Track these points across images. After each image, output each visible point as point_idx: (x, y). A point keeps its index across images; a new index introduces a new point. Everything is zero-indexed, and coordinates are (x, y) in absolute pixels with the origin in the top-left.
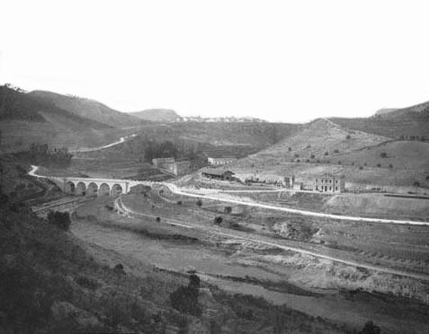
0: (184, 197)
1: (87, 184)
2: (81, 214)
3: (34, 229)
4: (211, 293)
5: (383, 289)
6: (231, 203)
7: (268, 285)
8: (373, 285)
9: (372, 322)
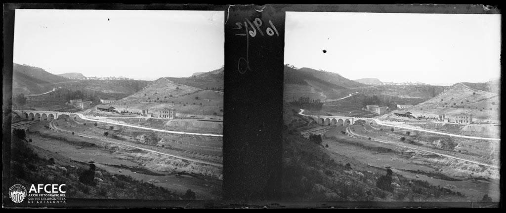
0: (384, 126)
1: (331, 119)
2: (328, 136)
3: (302, 144)
4: (398, 180)
5: (196, 171)
6: (113, 124)
7: (134, 169)
8: (192, 170)
9: (190, 190)
